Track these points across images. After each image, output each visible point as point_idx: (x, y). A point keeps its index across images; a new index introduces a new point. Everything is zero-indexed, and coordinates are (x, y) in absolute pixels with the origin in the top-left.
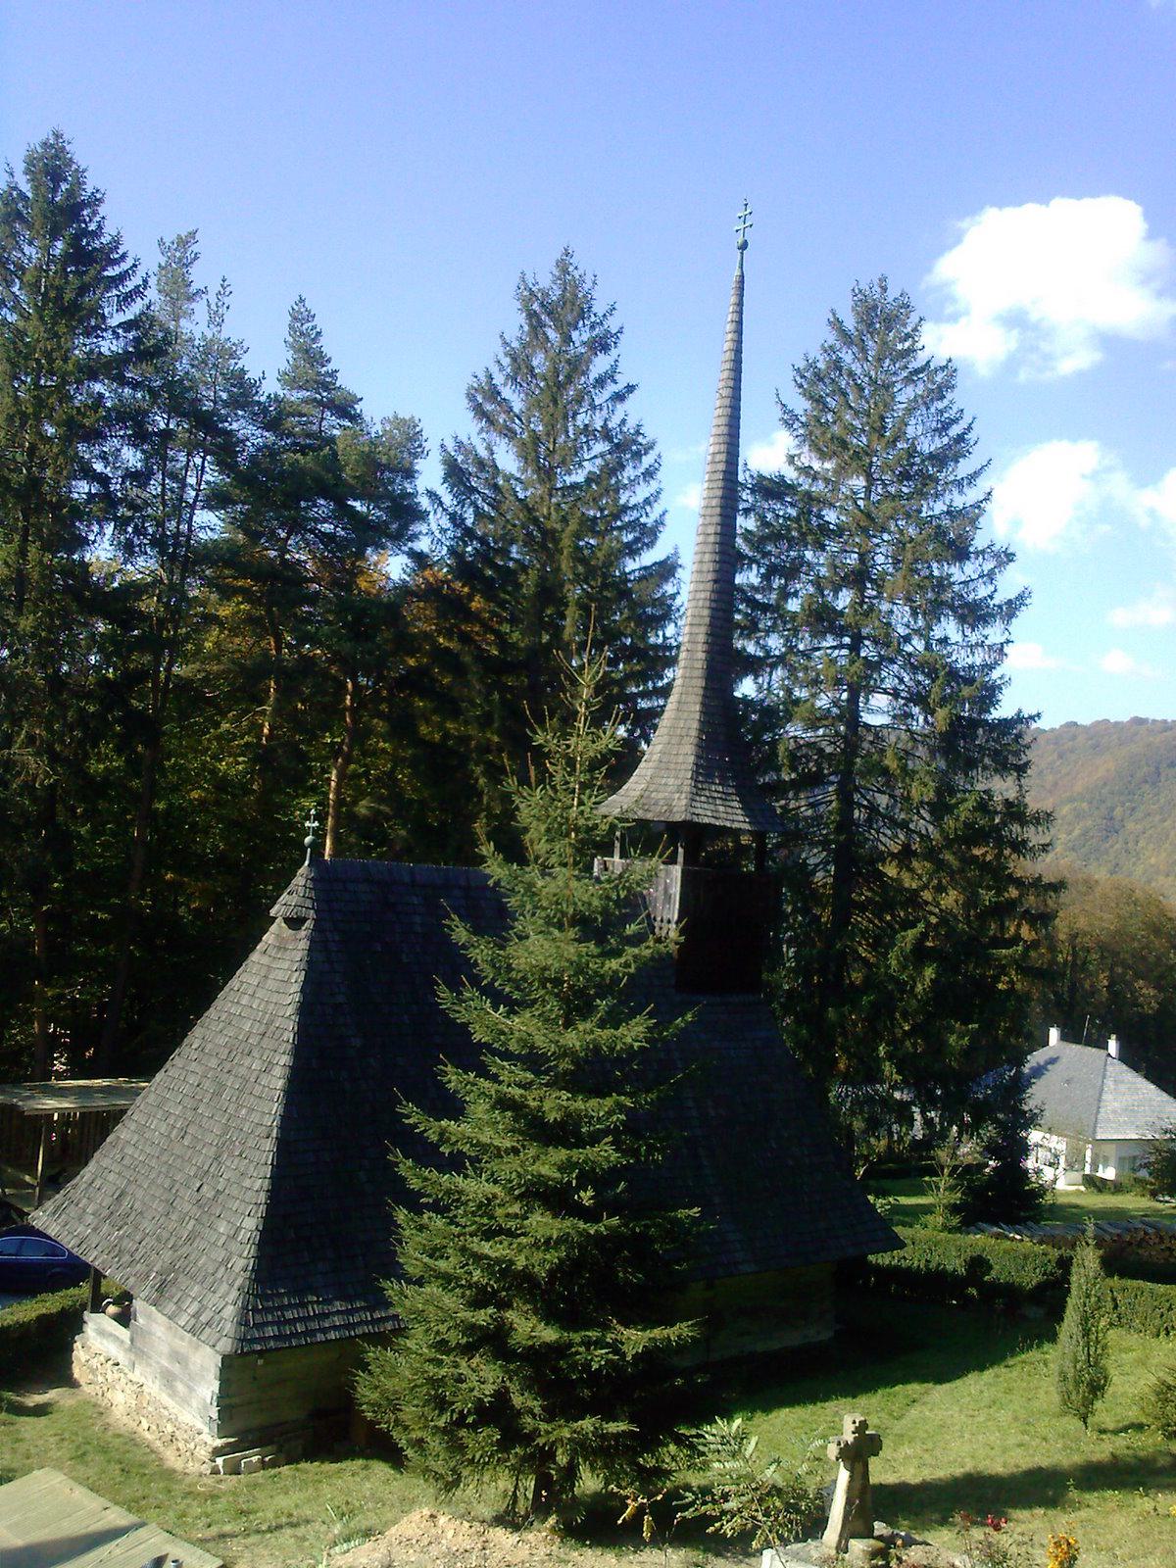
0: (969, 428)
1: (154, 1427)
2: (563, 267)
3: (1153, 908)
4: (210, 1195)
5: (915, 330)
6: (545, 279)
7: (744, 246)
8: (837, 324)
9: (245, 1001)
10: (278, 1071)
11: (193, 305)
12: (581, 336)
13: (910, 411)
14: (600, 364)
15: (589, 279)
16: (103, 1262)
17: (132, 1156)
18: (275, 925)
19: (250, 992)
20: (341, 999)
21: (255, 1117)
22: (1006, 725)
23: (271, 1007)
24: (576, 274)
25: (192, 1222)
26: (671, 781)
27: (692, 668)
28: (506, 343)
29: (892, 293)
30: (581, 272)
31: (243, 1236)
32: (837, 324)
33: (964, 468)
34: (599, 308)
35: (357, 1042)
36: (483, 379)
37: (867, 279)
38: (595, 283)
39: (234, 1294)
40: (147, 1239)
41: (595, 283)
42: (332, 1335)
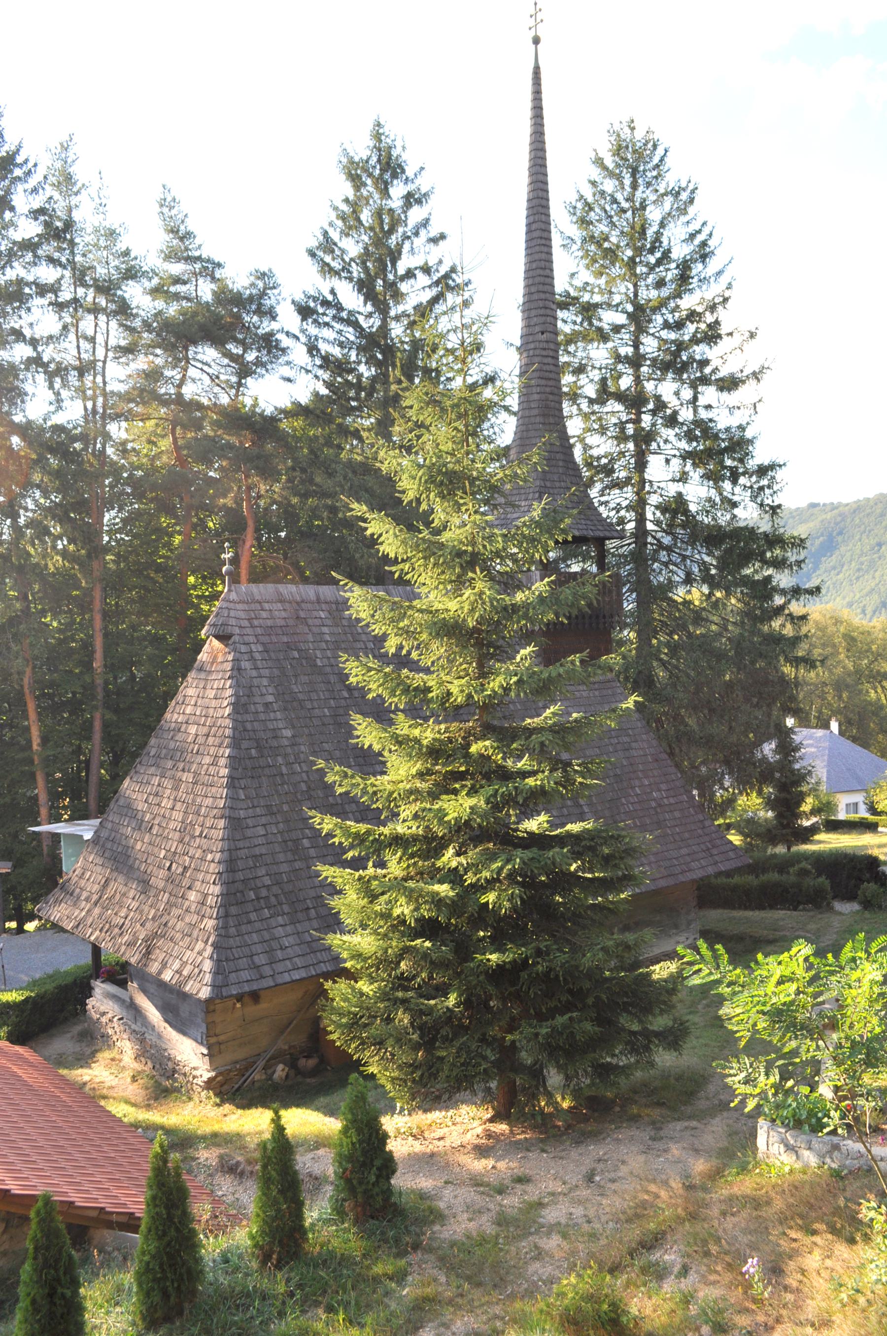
0: (710, 235)
1: (158, 1066)
2: (378, 136)
3: (170, 1064)
4: (180, 870)
5: (662, 160)
6: (362, 149)
7: (536, 41)
8: (599, 162)
9: (189, 710)
10: (223, 762)
11: (79, 198)
12: (398, 190)
13: (662, 225)
14: (415, 215)
15: (399, 144)
16: (97, 938)
17: (111, 850)
18: (206, 646)
19: (193, 703)
20: (270, 699)
21: (209, 802)
22: (213, 1070)
23: (211, 711)
24: (388, 141)
25: (167, 895)
26: (523, 504)
27: (530, 408)
28: (336, 209)
29: (639, 134)
30: (392, 138)
31: (211, 901)
32: (599, 162)
33: (714, 265)
34: (410, 172)
35: (288, 733)
36: (321, 238)
37: (618, 118)
38: (404, 148)
39: (209, 950)
40: (132, 914)
41: (404, 148)
42: (296, 976)
